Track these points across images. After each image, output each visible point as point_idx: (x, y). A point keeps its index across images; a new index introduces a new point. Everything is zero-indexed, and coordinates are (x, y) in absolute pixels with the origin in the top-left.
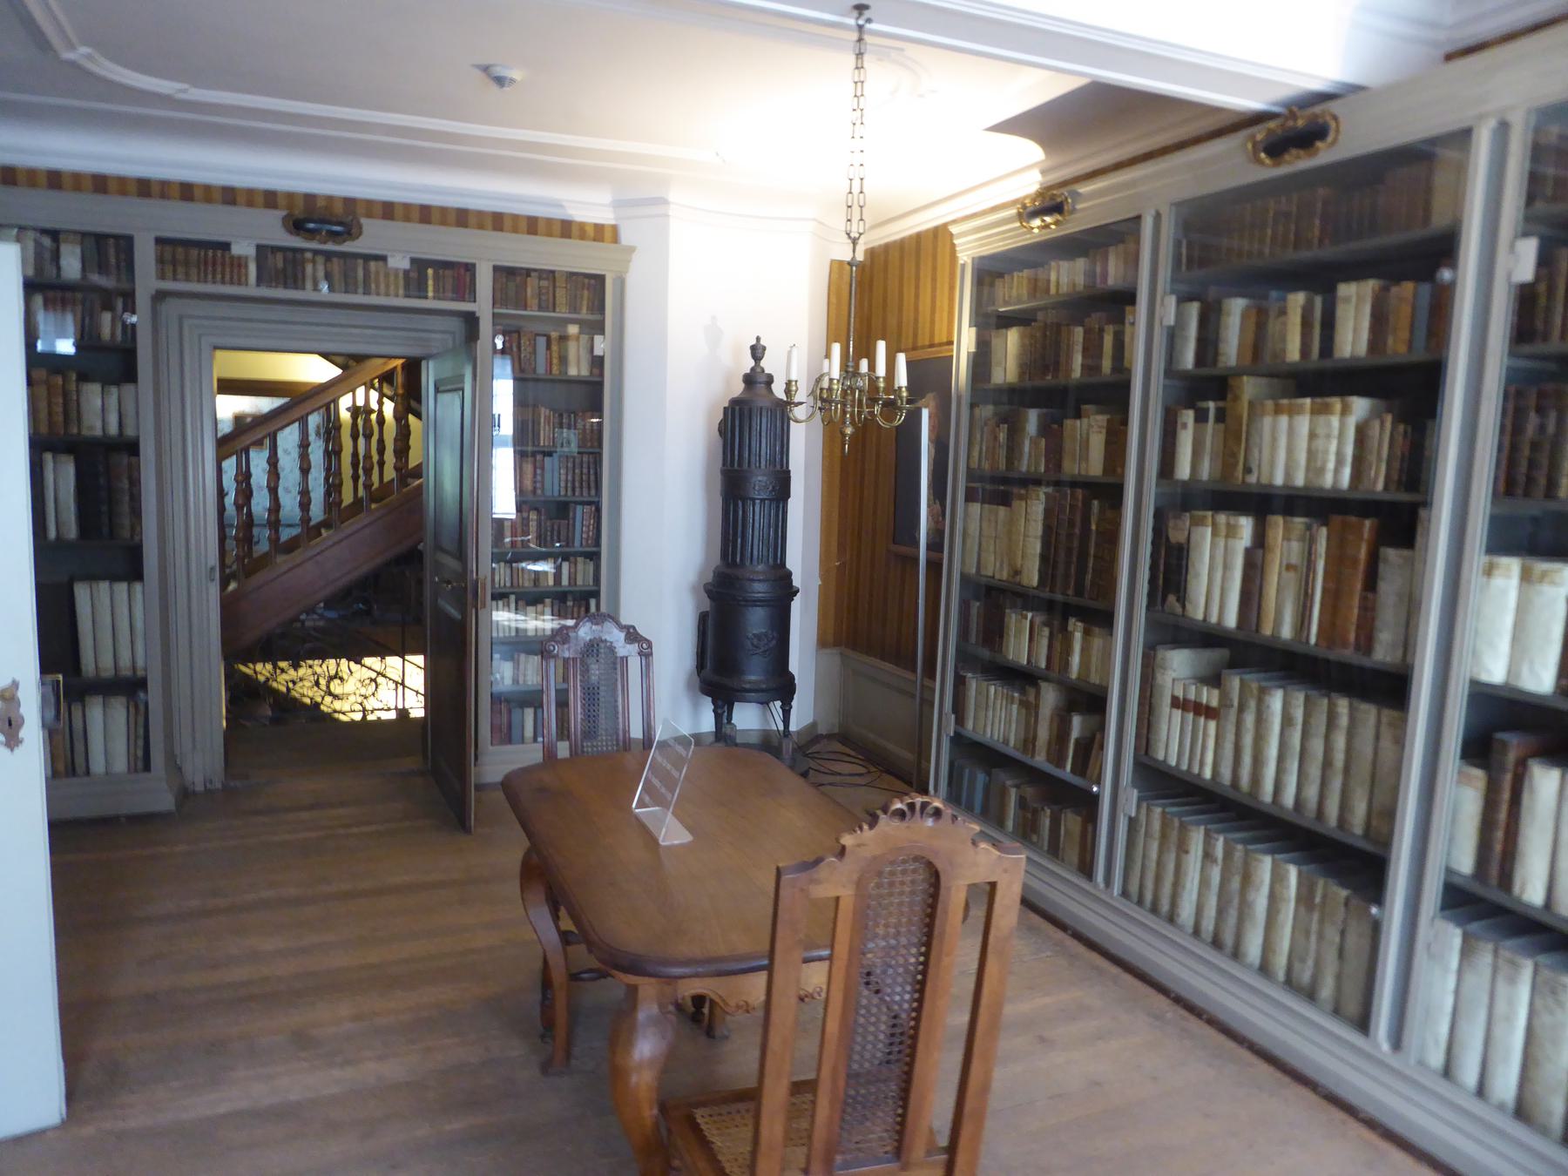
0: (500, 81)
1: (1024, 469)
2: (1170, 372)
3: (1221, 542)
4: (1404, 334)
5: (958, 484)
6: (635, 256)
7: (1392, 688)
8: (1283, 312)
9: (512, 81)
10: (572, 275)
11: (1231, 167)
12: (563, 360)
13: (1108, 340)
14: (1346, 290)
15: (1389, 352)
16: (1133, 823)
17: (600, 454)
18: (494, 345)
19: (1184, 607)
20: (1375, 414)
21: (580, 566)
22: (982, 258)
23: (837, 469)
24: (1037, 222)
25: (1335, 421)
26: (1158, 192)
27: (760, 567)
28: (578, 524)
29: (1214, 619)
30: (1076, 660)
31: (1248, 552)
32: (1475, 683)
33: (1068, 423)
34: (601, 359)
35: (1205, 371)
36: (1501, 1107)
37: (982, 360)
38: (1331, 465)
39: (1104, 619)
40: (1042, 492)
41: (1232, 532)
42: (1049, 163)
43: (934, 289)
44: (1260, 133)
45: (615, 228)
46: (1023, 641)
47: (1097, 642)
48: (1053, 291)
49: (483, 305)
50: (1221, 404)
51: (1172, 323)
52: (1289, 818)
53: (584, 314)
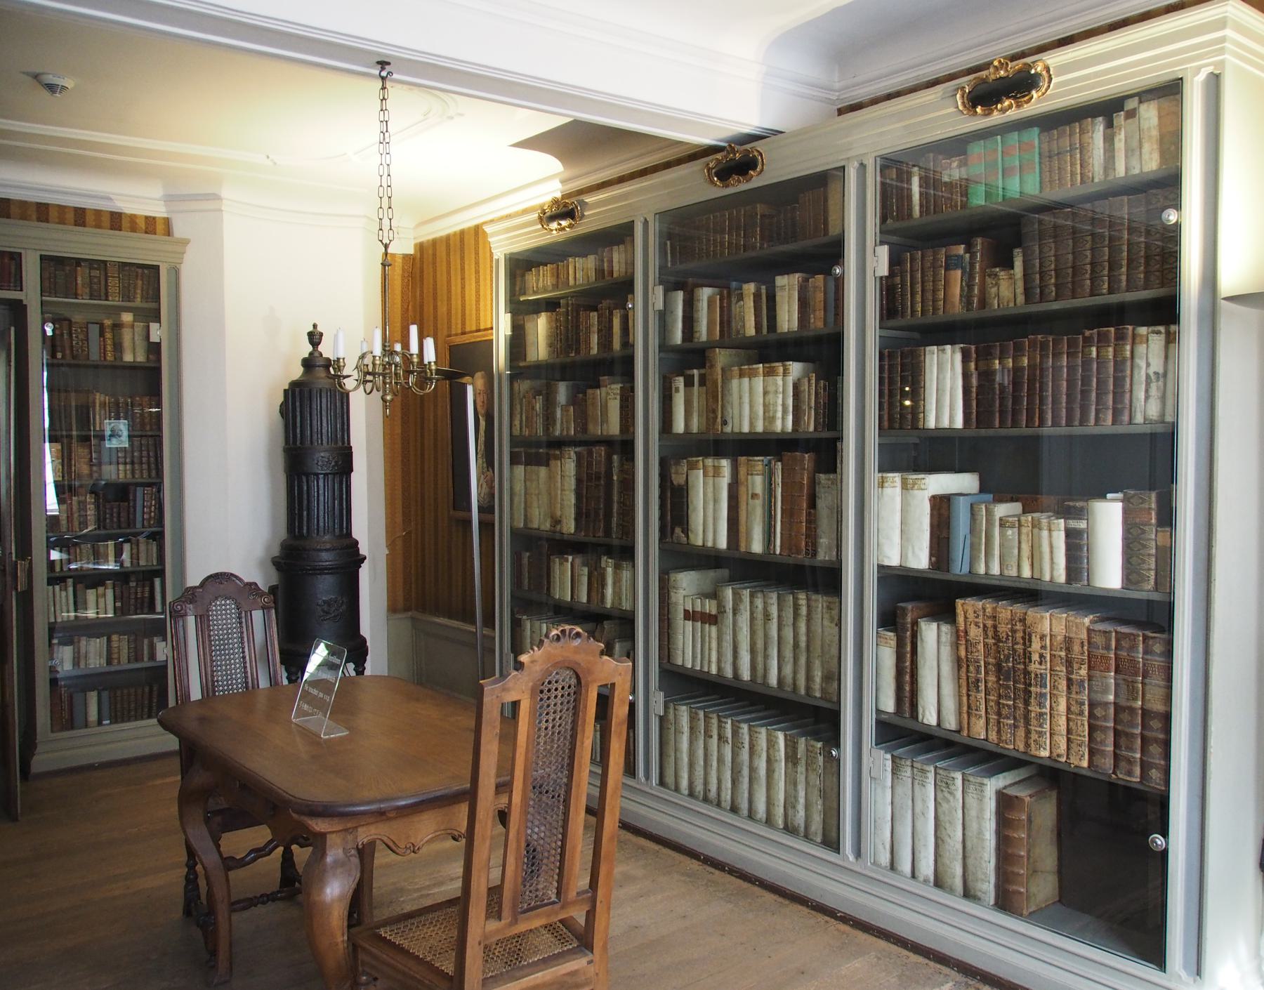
0: (52, 88)
1: (557, 433)
2: (664, 347)
3: (710, 480)
4: (820, 314)
5: (503, 449)
6: (190, 250)
7: (827, 580)
8: (741, 297)
9: (64, 88)
10: (124, 265)
11: (693, 186)
12: (118, 347)
13: (617, 322)
14: (781, 281)
15: (812, 326)
16: (662, 720)
17: (160, 437)
18: (44, 331)
19: (688, 537)
20: (806, 374)
21: (142, 547)
22: (512, 254)
23: (398, 447)
24: (554, 225)
25: (779, 380)
26: (645, 203)
27: (327, 537)
28: (139, 509)
29: (710, 544)
30: (609, 591)
31: (730, 486)
32: (881, 567)
33: (590, 391)
34: (158, 345)
35: (688, 345)
36: (926, 881)
37: (518, 342)
38: (779, 415)
39: (626, 553)
40: (571, 453)
41: (717, 472)
42: (568, 174)
43: (478, 282)
44: (712, 160)
45: (167, 222)
46: (568, 580)
47: (626, 575)
48: (571, 282)
49: (31, 293)
50: (703, 371)
51: (662, 308)
52: (774, 694)
53: (138, 302)
